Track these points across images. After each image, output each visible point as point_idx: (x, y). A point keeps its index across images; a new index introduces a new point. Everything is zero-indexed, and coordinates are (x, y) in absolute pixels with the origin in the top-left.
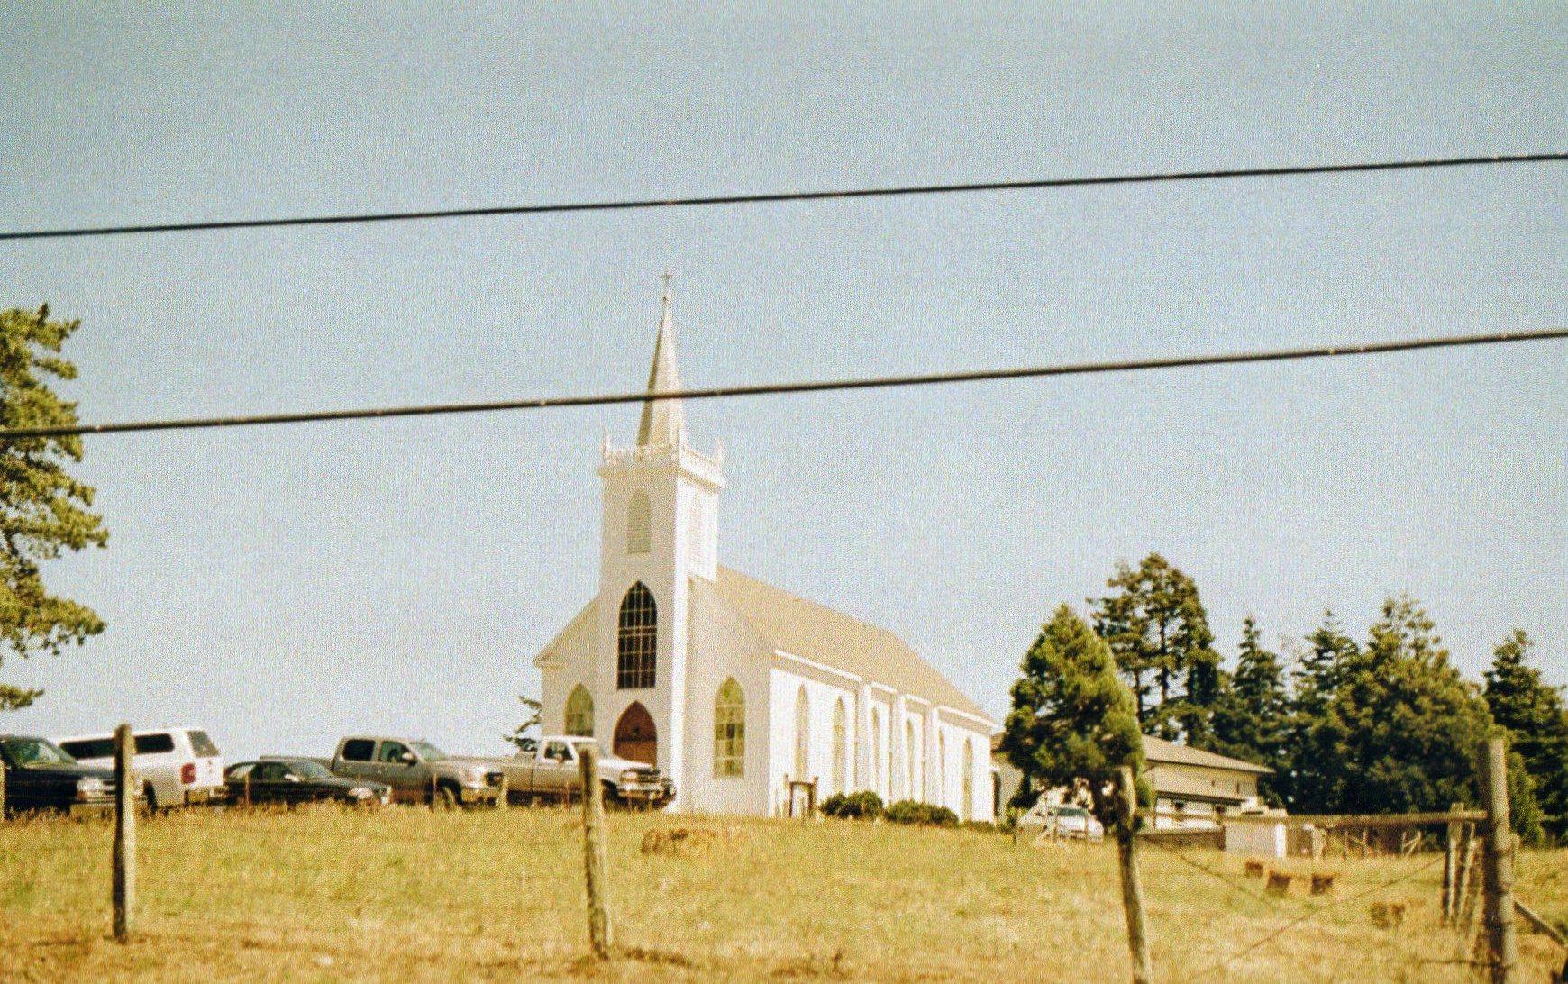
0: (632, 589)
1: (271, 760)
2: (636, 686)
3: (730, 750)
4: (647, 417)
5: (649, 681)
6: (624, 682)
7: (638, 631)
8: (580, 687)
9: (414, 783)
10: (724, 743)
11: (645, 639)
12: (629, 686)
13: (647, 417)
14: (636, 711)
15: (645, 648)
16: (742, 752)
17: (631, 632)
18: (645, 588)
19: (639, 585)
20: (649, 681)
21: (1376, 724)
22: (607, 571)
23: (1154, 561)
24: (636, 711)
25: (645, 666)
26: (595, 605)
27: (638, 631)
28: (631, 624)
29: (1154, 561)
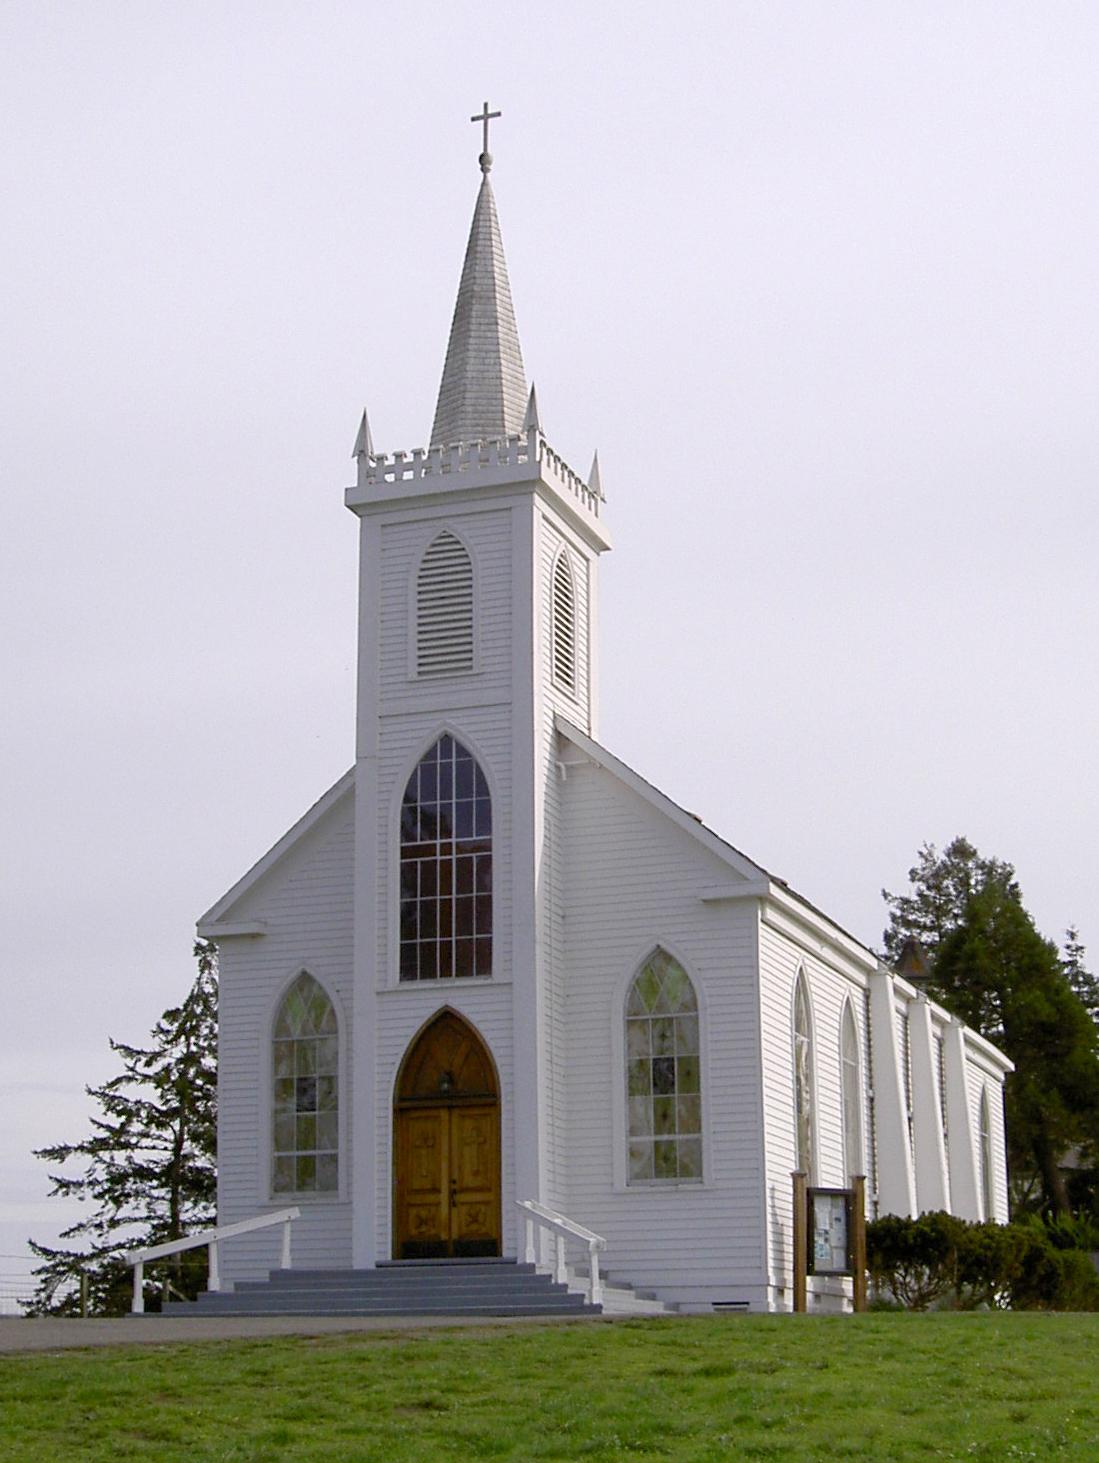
0: (430, 754)
1: (256, 1281)
2: (446, 972)
3: (664, 1117)
4: (486, 125)
5: (476, 960)
6: (417, 963)
7: (446, 849)
8: (305, 980)
9: (931, 1297)
10: (646, 1105)
11: (464, 865)
12: (428, 973)
13: (486, 125)
14: (447, 1025)
15: (464, 885)
16: (694, 1123)
17: (430, 850)
18: (462, 751)
19: (446, 739)
20: (476, 960)
21: (206, 1106)
22: (374, 715)
23: (961, 850)
24: (447, 1025)
25: (465, 927)
26: (338, 805)
27: (446, 849)
28: (430, 833)
29: (961, 850)
